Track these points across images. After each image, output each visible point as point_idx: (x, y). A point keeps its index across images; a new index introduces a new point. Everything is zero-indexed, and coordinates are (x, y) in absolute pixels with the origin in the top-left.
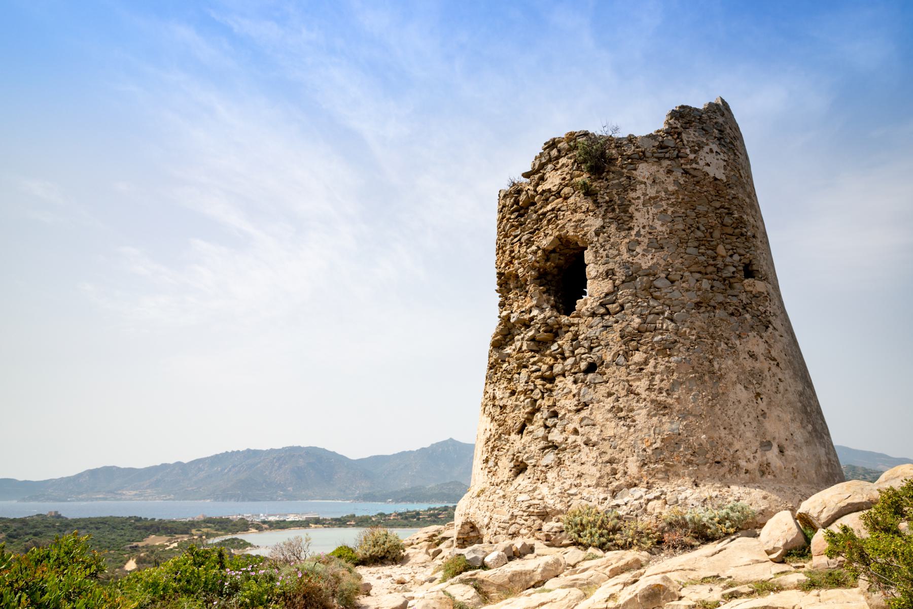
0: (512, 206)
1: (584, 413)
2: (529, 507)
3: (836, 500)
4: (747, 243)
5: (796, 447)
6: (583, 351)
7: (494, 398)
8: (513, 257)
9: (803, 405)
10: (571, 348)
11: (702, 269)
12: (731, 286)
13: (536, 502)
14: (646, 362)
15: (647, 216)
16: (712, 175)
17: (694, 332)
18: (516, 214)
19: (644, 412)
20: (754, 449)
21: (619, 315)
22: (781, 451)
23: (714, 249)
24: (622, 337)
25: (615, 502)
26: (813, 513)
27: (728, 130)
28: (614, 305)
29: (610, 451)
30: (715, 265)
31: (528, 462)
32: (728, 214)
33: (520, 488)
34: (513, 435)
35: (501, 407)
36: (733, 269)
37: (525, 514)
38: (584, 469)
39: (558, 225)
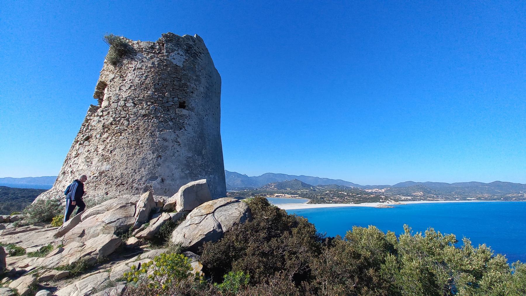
14: (107, 138)
19: (97, 159)
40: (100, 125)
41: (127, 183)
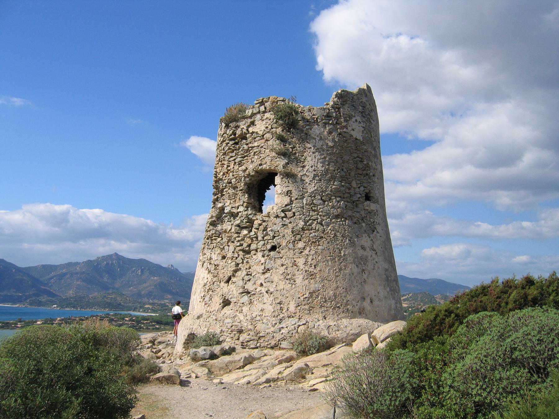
0: (231, 135)
1: (267, 275)
2: (232, 326)
3: (388, 330)
5: (380, 300)
7: (211, 259)
9: (387, 277)
10: (262, 236)
11: (342, 195)
12: (357, 206)
13: (236, 324)
14: (304, 248)
17: (333, 232)
18: (233, 142)
19: (301, 277)
20: (357, 300)
22: (371, 302)
23: (350, 183)
24: (293, 233)
25: (281, 326)
27: (368, 106)
29: (280, 297)
30: (349, 193)
31: (231, 300)
32: (361, 161)
35: (215, 265)
37: (230, 330)
38: (265, 307)
39: (260, 157)
41: (341, 305)
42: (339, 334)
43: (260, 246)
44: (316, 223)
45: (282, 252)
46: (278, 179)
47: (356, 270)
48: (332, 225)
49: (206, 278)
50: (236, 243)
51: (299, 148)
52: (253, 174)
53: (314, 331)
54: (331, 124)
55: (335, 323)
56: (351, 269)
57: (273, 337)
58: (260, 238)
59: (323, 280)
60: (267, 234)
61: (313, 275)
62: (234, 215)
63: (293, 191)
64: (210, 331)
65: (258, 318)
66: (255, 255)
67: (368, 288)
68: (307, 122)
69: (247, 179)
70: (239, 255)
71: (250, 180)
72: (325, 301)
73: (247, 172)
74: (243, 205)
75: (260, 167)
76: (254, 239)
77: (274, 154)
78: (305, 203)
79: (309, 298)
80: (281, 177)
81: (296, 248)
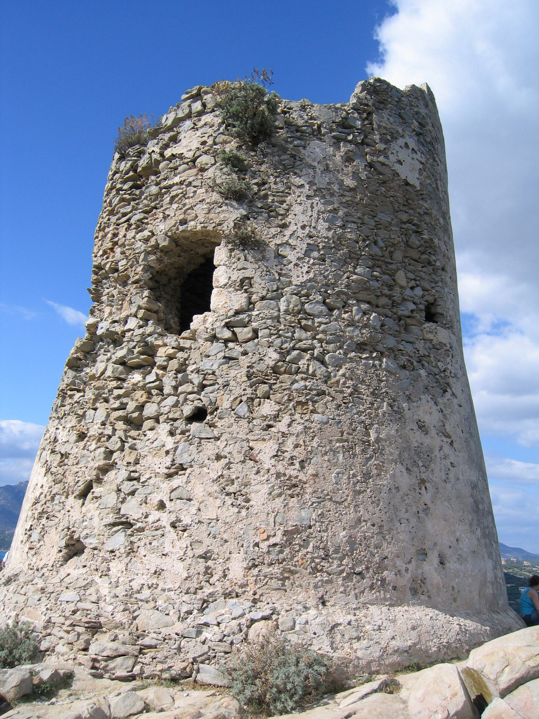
0: (127, 173)
1: (177, 481)
2: (74, 612)
3: (523, 655)
4: (433, 276)
5: (461, 559)
6: (190, 389)
7: (56, 440)
8: (116, 243)
9: (475, 502)
10: (174, 383)
11: (372, 298)
12: (406, 328)
13: (87, 605)
14: (276, 417)
15: (309, 213)
16: (403, 177)
17: (350, 383)
18: (130, 184)
19: (265, 489)
20: (409, 557)
21: (250, 343)
22: (442, 563)
23: (392, 275)
24: (249, 377)
25: (203, 619)
26: (489, 672)
27: (430, 127)
28: (246, 329)
29: (207, 541)
30: (390, 297)
32: (416, 232)
33: (67, 580)
34: (71, 498)
35: (62, 455)
36: (412, 306)
37: (68, 622)
39: (184, 205)
40: (238, 374)
41: (367, 568)
42: (363, 651)
43: (167, 409)
44: (308, 356)
45: (219, 424)
46: (220, 255)
47: (406, 481)
48: (348, 365)
49: (39, 486)
50: (112, 401)
51: (274, 184)
52: (166, 243)
53: (293, 638)
54: (350, 142)
55: (350, 617)
56: (393, 476)
57: (179, 649)
58: (167, 390)
59: (321, 500)
60: (186, 381)
61: (295, 486)
62: (116, 340)
63: (257, 279)
64: (23, 618)
65: (146, 593)
66: (152, 429)
67: (434, 527)
68: (297, 131)
69: (152, 257)
70: (114, 430)
71: (159, 260)
72: (326, 557)
73: (152, 242)
74: (135, 316)
75: (181, 228)
76: (154, 392)
77: (215, 196)
78: (283, 307)
79: (283, 546)
80: (230, 246)
81: (254, 415)
